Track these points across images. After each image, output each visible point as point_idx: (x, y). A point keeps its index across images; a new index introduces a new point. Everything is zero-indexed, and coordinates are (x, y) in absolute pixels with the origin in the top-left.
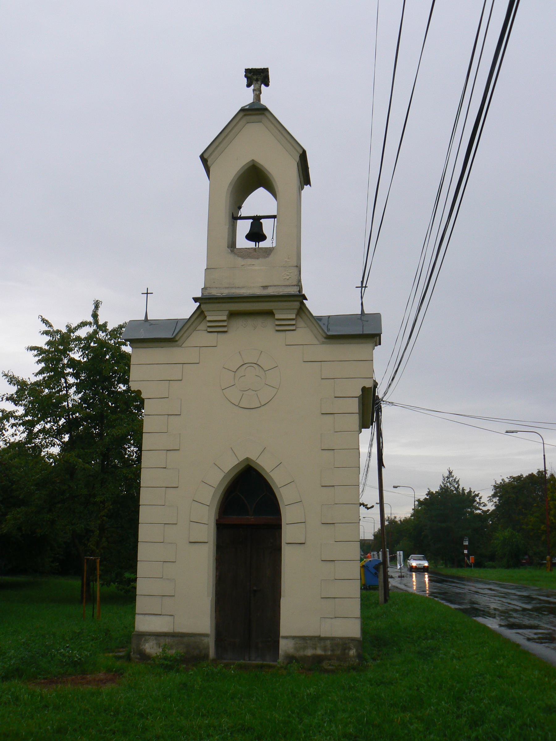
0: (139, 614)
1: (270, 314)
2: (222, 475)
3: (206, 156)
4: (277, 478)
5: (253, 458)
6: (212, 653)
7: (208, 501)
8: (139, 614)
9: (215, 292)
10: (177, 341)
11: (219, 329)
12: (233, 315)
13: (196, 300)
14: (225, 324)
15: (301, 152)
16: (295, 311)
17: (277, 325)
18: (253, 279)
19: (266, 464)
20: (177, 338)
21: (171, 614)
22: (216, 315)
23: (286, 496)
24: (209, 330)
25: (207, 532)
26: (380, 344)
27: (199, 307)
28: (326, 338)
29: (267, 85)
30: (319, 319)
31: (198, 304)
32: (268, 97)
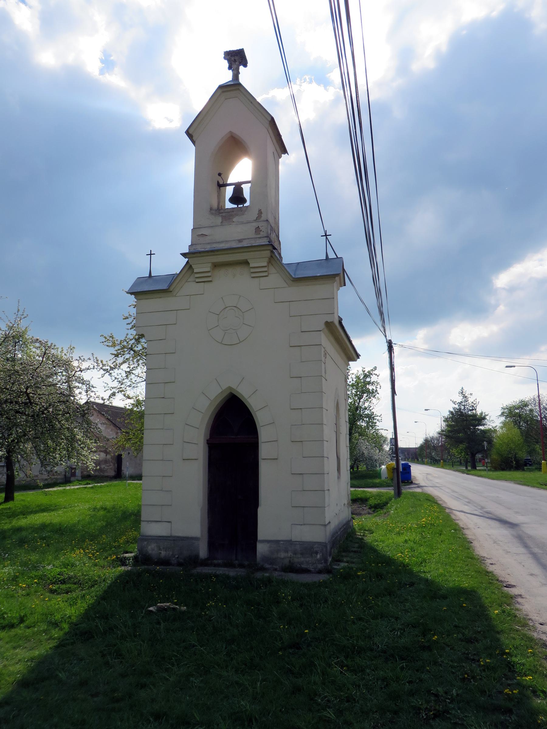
0: (143, 521)
1: (246, 263)
2: (220, 391)
3: (190, 132)
4: (254, 403)
5: (234, 386)
7: (212, 398)
8: (143, 521)
9: (199, 248)
10: (171, 292)
11: (205, 279)
12: (216, 266)
13: (184, 255)
14: (209, 274)
15: (270, 119)
16: (267, 259)
17: (252, 273)
20: (171, 289)
21: (169, 520)
23: (261, 418)
24: (198, 280)
25: (199, 451)
26: (345, 285)
27: (188, 262)
28: (293, 281)
29: (245, 65)
31: (187, 259)
32: (246, 77)
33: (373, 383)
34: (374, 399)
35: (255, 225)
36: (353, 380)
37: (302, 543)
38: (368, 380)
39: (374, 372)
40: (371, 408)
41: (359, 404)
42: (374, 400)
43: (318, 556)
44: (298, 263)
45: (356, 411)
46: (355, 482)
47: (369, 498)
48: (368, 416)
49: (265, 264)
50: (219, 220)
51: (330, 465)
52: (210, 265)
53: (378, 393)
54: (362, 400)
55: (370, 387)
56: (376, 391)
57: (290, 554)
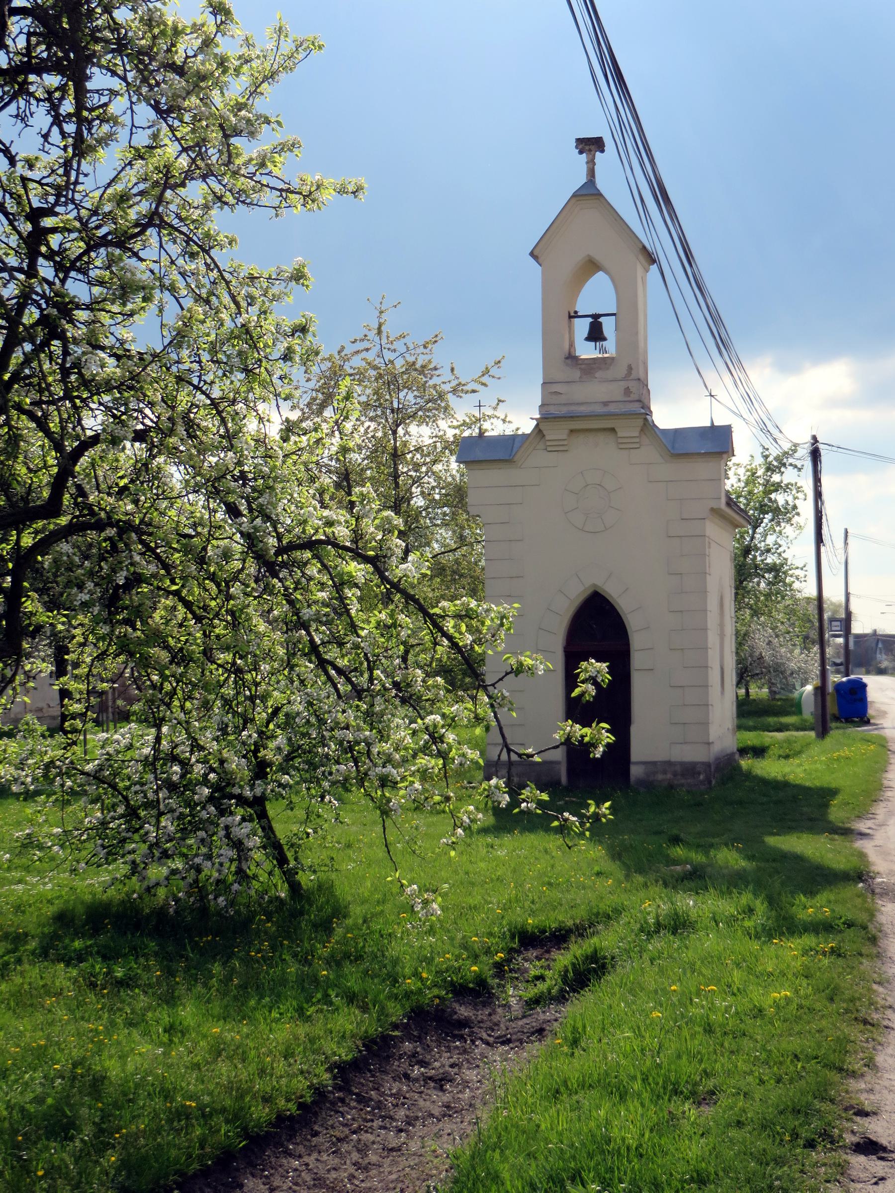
1: (613, 430)
2: (582, 588)
4: (624, 604)
6: (564, 779)
7: (629, 616)
9: (553, 410)
11: (560, 448)
14: (565, 443)
18: (595, 393)
19: (613, 592)
22: (554, 433)
23: (633, 622)
29: (603, 151)
30: (665, 432)
33: (787, 488)
34: (788, 526)
35: (623, 384)
36: (739, 480)
37: (682, 764)
38: (776, 478)
39: (791, 460)
40: (781, 550)
41: (753, 538)
42: (788, 530)
43: (701, 777)
44: (601, 195)
45: (745, 558)
46: (744, 721)
47: (768, 747)
48: (775, 569)
49: (637, 434)
50: (577, 374)
51: (714, 676)
52: (566, 432)
53: (798, 514)
54: (760, 530)
55: (780, 498)
56: (795, 507)
57: (669, 776)
